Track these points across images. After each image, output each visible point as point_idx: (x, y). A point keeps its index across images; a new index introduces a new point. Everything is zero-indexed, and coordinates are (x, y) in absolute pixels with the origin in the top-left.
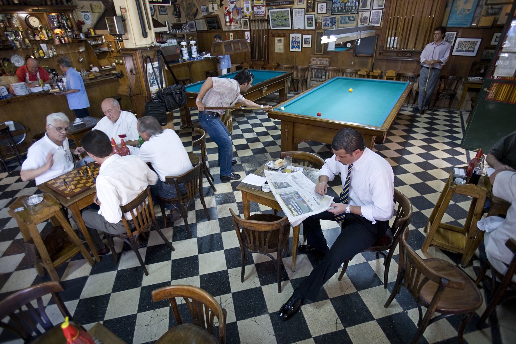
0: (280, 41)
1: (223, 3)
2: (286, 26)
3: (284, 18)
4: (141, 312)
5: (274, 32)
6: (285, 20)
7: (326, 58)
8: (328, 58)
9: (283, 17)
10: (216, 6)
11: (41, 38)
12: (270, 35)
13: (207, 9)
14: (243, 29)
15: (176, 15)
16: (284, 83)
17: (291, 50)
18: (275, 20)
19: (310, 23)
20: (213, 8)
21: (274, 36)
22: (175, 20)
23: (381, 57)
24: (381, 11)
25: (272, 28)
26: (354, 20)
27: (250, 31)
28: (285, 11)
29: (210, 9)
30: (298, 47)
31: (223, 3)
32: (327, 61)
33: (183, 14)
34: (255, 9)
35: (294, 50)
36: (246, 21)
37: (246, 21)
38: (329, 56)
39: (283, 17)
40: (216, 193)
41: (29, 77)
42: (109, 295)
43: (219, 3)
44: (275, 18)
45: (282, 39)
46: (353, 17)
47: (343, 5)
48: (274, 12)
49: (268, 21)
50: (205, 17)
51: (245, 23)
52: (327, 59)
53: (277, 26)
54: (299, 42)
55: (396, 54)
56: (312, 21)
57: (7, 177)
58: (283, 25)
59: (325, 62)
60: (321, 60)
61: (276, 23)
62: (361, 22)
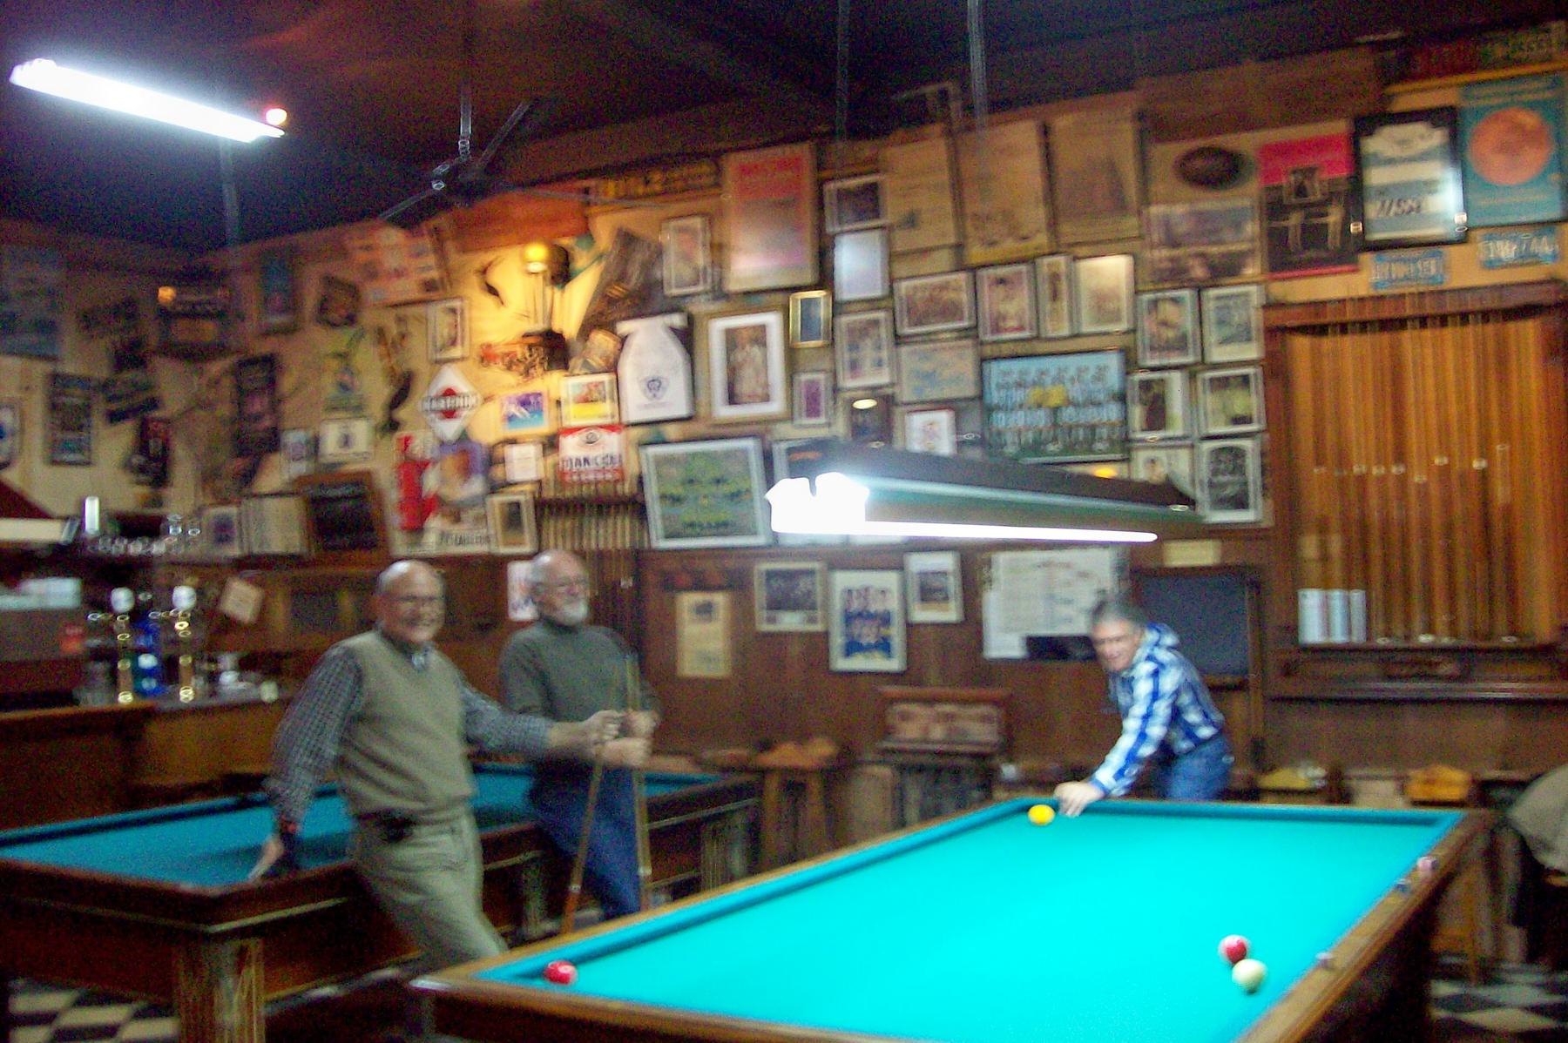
0: (705, 610)
2: (741, 531)
3: (725, 489)
5: (671, 565)
6: (735, 496)
7: (977, 701)
8: (995, 702)
10: (361, 431)
12: (651, 579)
13: (315, 444)
15: (142, 470)
16: (695, 848)
17: (841, 664)
18: (676, 500)
20: (346, 441)
21: (671, 585)
22: (130, 496)
23: (1288, 687)
24: (1247, 444)
28: (728, 455)
29: (331, 445)
30: (884, 646)
32: (985, 719)
33: (184, 471)
34: (571, 447)
35: (859, 663)
38: (999, 692)
40: (100, 407)
44: (678, 491)
45: (720, 599)
47: (1041, 419)
48: (669, 460)
49: (635, 507)
50: (296, 488)
51: (512, 517)
52: (984, 709)
53: (693, 529)
54: (885, 619)
58: (723, 528)
59: (979, 729)
60: (950, 717)
61: (686, 513)
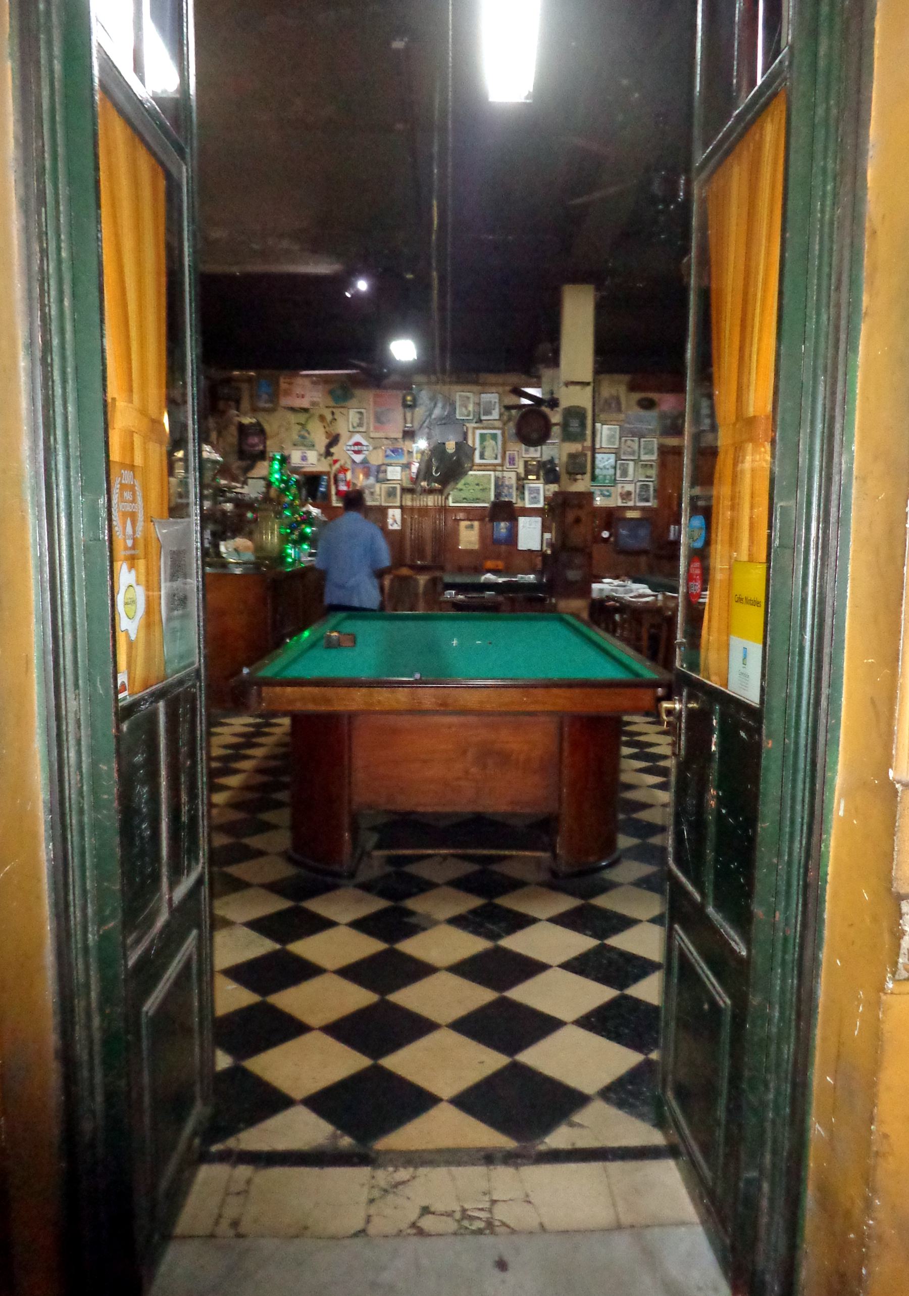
0: (471, 527)
1: (332, 450)
3: (481, 487)
4: (621, 1104)
6: (483, 490)
9: (478, 485)
11: (471, 514)
14: (383, 504)
19: (535, 497)
25: (451, 504)
26: (609, 496)
27: (401, 507)
31: (332, 450)
36: (395, 488)
37: (395, 488)
39: (478, 485)
41: (720, 773)
42: (441, 1100)
43: (322, 450)
46: (608, 491)
55: (699, 544)
56: (538, 494)
57: (415, 1235)
62: (623, 499)
